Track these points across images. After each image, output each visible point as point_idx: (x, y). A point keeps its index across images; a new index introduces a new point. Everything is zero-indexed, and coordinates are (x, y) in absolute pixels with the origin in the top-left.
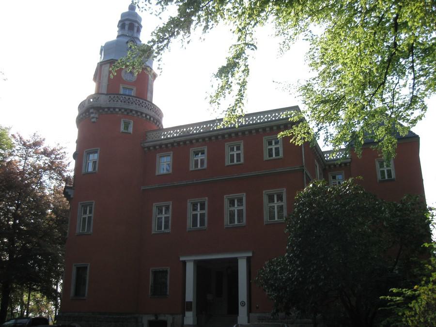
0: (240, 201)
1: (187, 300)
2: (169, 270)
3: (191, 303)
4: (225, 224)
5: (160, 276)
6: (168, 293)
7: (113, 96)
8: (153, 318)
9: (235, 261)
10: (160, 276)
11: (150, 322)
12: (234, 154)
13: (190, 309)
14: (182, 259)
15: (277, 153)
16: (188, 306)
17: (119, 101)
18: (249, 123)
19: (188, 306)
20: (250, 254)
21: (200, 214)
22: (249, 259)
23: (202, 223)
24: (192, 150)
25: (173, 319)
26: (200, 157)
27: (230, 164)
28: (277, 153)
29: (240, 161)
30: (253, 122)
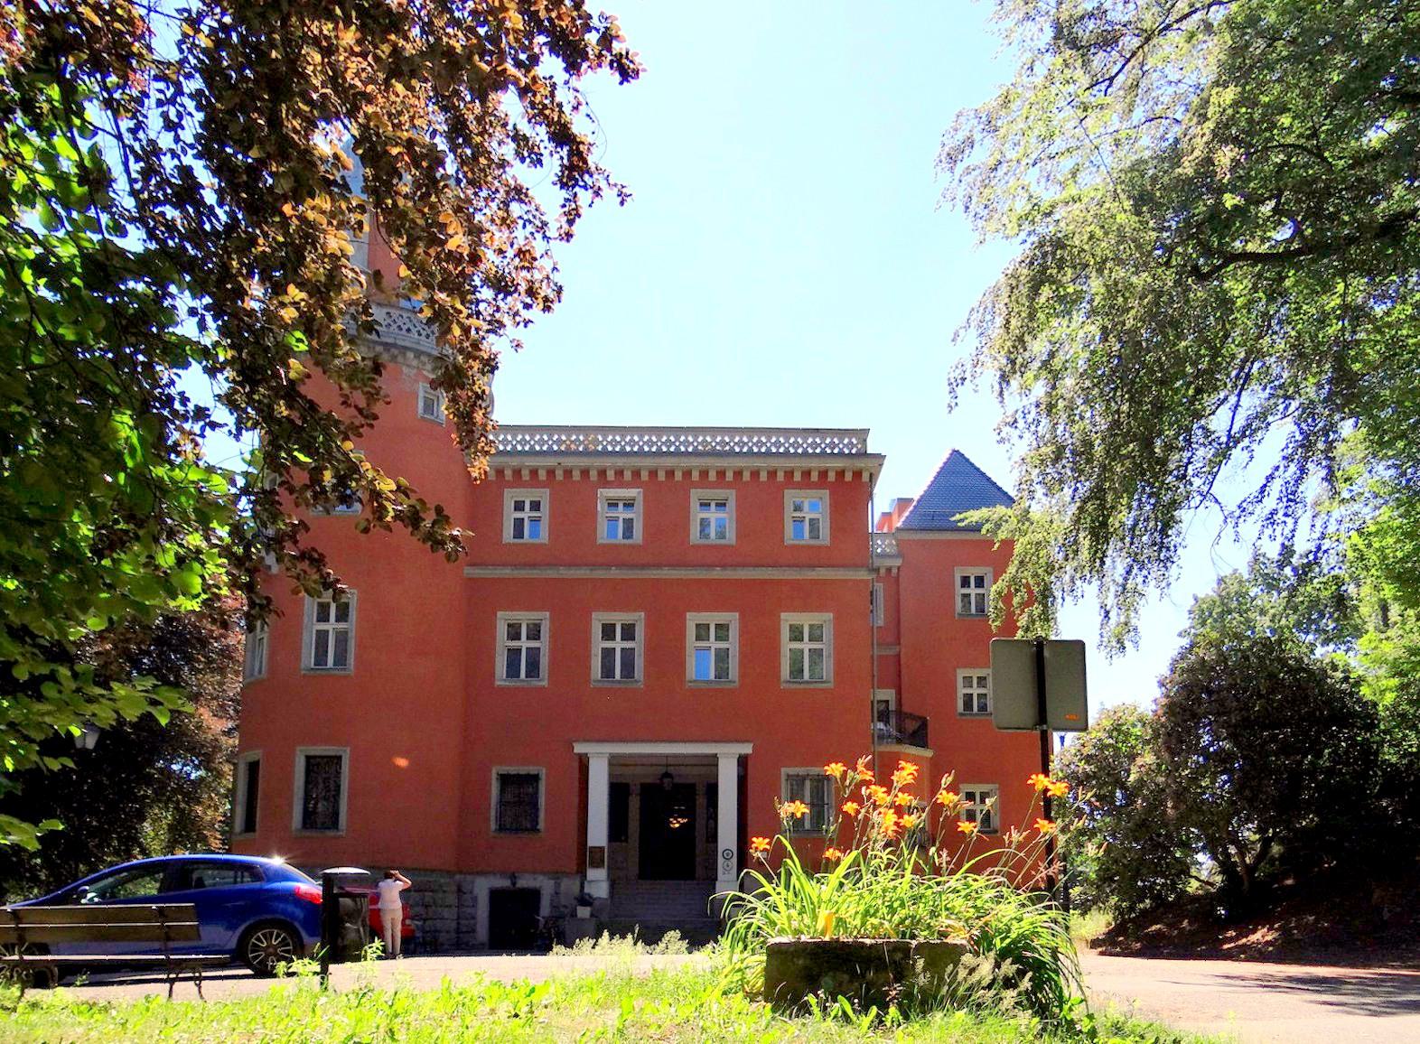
0: (722, 630)
1: (591, 843)
2: (543, 777)
3: (601, 849)
4: (303, 666)
5: (519, 789)
6: (541, 825)
7: (398, 312)
8: (504, 883)
9: (712, 762)
10: (519, 789)
11: (495, 895)
12: (617, 519)
13: (598, 864)
14: (579, 748)
15: (628, 532)
16: (596, 857)
17: (414, 330)
18: (769, 449)
19: (596, 857)
20: (747, 749)
21: (623, 650)
22: (743, 761)
23: (341, 659)
24: (696, 495)
25: (558, 885)
26: (713, 515)
27: (512, 540)
28: (628, 532)
29: (631, 537)
30: (686, 447)
